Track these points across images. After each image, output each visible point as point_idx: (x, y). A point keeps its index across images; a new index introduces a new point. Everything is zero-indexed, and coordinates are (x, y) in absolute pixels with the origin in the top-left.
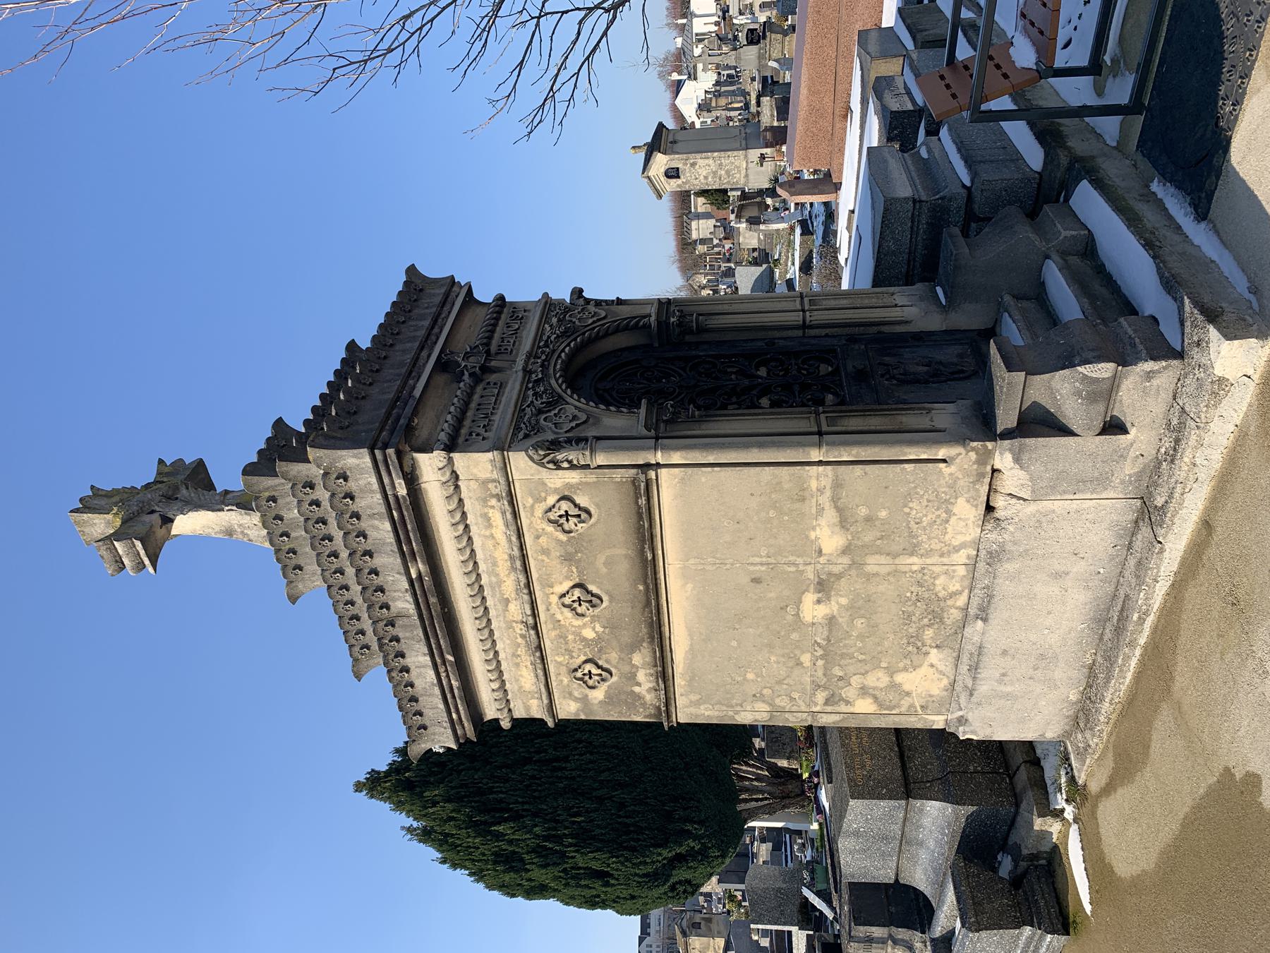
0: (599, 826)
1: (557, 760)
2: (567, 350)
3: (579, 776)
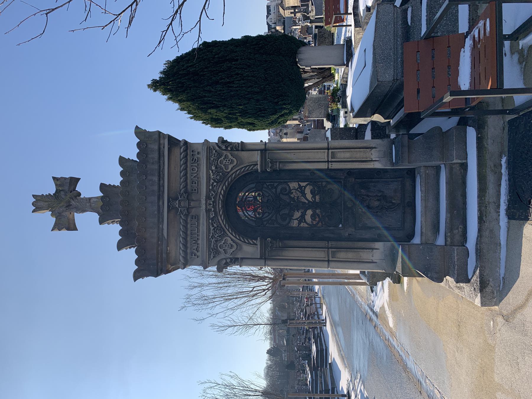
1: (229, 83)
2: (222, 192)
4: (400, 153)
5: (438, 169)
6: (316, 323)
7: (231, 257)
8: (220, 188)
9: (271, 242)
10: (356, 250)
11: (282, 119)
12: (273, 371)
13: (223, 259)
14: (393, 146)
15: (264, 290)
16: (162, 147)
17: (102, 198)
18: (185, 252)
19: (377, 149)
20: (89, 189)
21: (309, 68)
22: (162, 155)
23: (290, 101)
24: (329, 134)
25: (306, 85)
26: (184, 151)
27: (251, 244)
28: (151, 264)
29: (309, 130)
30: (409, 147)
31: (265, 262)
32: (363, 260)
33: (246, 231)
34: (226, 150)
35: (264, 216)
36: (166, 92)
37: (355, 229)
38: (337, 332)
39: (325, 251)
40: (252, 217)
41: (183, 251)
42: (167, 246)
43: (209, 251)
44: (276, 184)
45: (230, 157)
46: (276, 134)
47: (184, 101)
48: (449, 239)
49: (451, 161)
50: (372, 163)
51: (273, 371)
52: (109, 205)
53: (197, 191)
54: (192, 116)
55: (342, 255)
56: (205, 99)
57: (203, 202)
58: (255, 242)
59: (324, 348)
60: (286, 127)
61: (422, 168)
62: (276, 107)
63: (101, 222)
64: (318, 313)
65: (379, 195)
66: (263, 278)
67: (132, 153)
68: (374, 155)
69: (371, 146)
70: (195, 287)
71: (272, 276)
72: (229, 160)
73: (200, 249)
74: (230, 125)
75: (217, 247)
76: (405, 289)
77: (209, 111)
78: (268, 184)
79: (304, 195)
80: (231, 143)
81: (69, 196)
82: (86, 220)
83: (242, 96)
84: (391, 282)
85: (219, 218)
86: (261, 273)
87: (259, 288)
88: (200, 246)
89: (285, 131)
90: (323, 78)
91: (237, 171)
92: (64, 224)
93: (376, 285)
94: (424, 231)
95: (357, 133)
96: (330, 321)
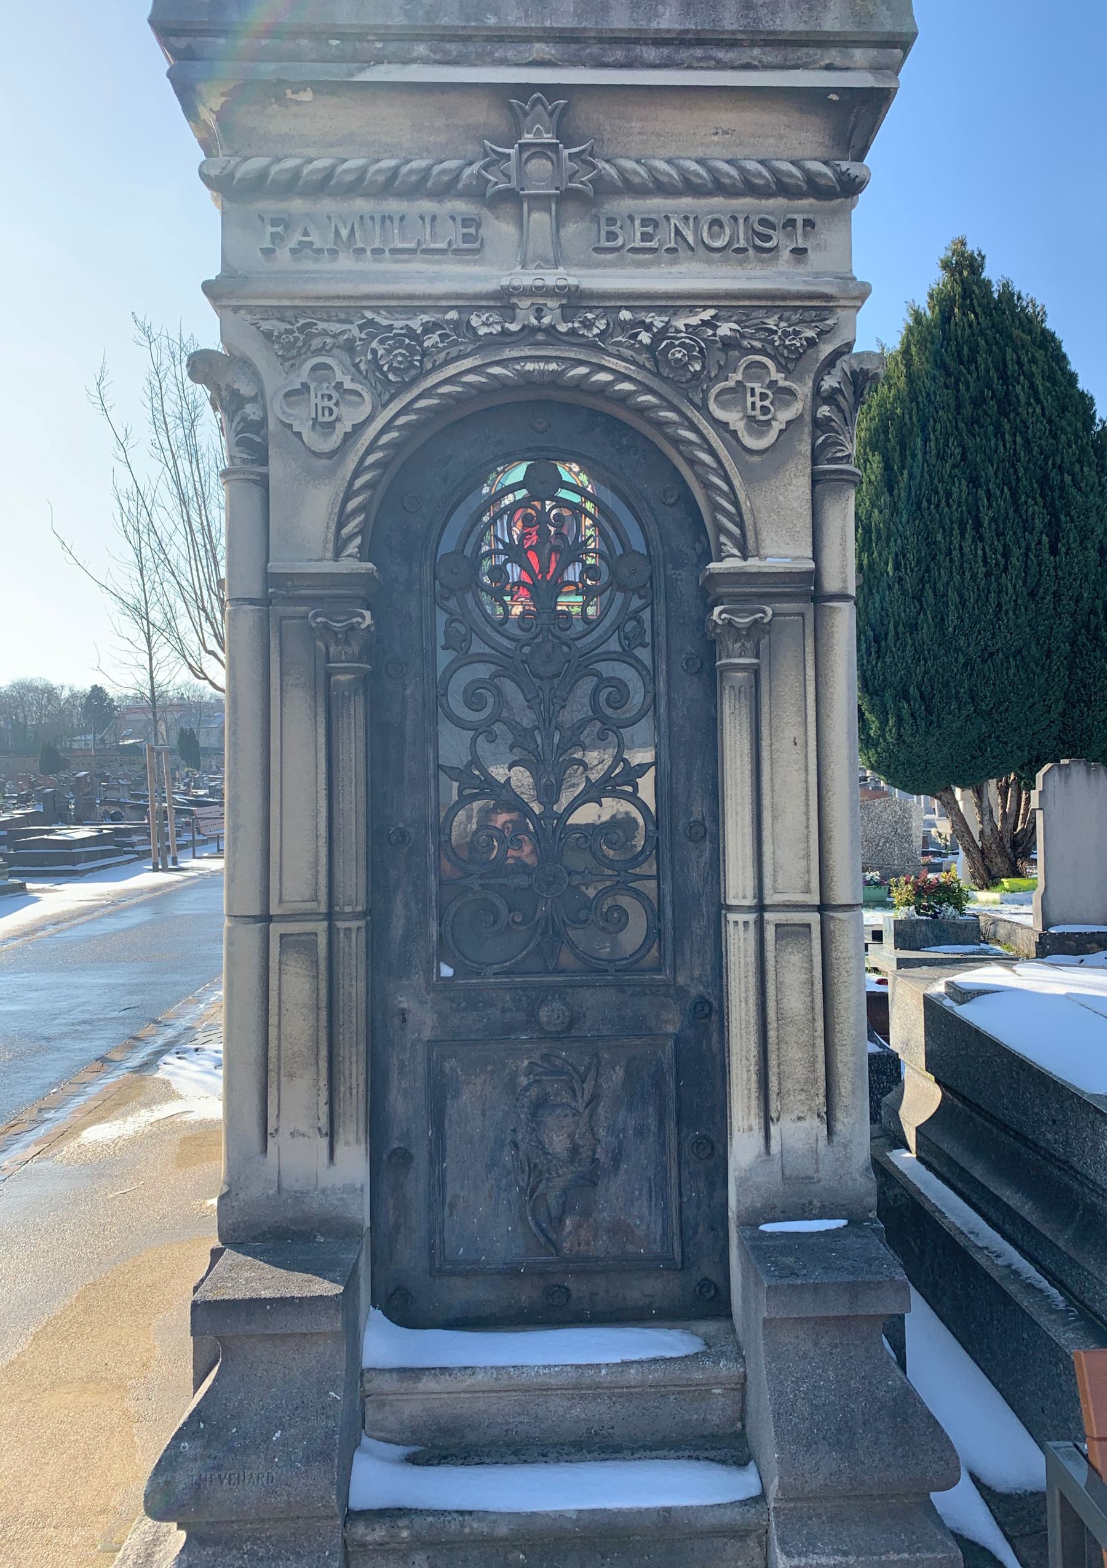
0: (883, 599)
1: (978, 525)
2: (603, 377)
3: (952, 561)
5: (728, 1447)
6: (163, 837)
7: (272, 426)
9: (352, 627)
10: (324, 1052)
12: (40, 707)
13: (256, 377)
14: (843, 1223)
16: (833, 56)
18: (291, 186)
19: (822, 1144)
21: (1035, 803)
22: (793, 54)
23: (909, 740)
25: (958, 792)
26: (810, 178)
27: (340, 526)
30: (842, 1322)
31: (251, 601)
32: (272, 1091)
33: (411, 504)
34: (819, 397)
36: (940, 302)
38: (123, 910)
39: (315, 899)
43: (301, 311)
44: (644, 654)
45: (784, 416)
47: (908, 366)
48: (379, 1533)
49: (782, 1541)
50: (756, 1123)
51: (40, 707)
53: (608, 250)
55: (297, 986)
56: (919, 442)
57: (551, 278)
58: (352, 548)
59: (80, 867)
61: (736, 1369)
62: (888, 694)
64: (204, 842)
68: (798, 1131)
69: (840, 1114)
72: (765, 410)
73: (308, 265)
75: (318, 352)
77: (876, 459)
78: (646, 615)
79: (594, 793)
83: (928, 570)
85: (468, 363)
88: (325, 265)
90: (982, 852)
91: (712, 452)
94: (427, 1384)
96: (169, 885)
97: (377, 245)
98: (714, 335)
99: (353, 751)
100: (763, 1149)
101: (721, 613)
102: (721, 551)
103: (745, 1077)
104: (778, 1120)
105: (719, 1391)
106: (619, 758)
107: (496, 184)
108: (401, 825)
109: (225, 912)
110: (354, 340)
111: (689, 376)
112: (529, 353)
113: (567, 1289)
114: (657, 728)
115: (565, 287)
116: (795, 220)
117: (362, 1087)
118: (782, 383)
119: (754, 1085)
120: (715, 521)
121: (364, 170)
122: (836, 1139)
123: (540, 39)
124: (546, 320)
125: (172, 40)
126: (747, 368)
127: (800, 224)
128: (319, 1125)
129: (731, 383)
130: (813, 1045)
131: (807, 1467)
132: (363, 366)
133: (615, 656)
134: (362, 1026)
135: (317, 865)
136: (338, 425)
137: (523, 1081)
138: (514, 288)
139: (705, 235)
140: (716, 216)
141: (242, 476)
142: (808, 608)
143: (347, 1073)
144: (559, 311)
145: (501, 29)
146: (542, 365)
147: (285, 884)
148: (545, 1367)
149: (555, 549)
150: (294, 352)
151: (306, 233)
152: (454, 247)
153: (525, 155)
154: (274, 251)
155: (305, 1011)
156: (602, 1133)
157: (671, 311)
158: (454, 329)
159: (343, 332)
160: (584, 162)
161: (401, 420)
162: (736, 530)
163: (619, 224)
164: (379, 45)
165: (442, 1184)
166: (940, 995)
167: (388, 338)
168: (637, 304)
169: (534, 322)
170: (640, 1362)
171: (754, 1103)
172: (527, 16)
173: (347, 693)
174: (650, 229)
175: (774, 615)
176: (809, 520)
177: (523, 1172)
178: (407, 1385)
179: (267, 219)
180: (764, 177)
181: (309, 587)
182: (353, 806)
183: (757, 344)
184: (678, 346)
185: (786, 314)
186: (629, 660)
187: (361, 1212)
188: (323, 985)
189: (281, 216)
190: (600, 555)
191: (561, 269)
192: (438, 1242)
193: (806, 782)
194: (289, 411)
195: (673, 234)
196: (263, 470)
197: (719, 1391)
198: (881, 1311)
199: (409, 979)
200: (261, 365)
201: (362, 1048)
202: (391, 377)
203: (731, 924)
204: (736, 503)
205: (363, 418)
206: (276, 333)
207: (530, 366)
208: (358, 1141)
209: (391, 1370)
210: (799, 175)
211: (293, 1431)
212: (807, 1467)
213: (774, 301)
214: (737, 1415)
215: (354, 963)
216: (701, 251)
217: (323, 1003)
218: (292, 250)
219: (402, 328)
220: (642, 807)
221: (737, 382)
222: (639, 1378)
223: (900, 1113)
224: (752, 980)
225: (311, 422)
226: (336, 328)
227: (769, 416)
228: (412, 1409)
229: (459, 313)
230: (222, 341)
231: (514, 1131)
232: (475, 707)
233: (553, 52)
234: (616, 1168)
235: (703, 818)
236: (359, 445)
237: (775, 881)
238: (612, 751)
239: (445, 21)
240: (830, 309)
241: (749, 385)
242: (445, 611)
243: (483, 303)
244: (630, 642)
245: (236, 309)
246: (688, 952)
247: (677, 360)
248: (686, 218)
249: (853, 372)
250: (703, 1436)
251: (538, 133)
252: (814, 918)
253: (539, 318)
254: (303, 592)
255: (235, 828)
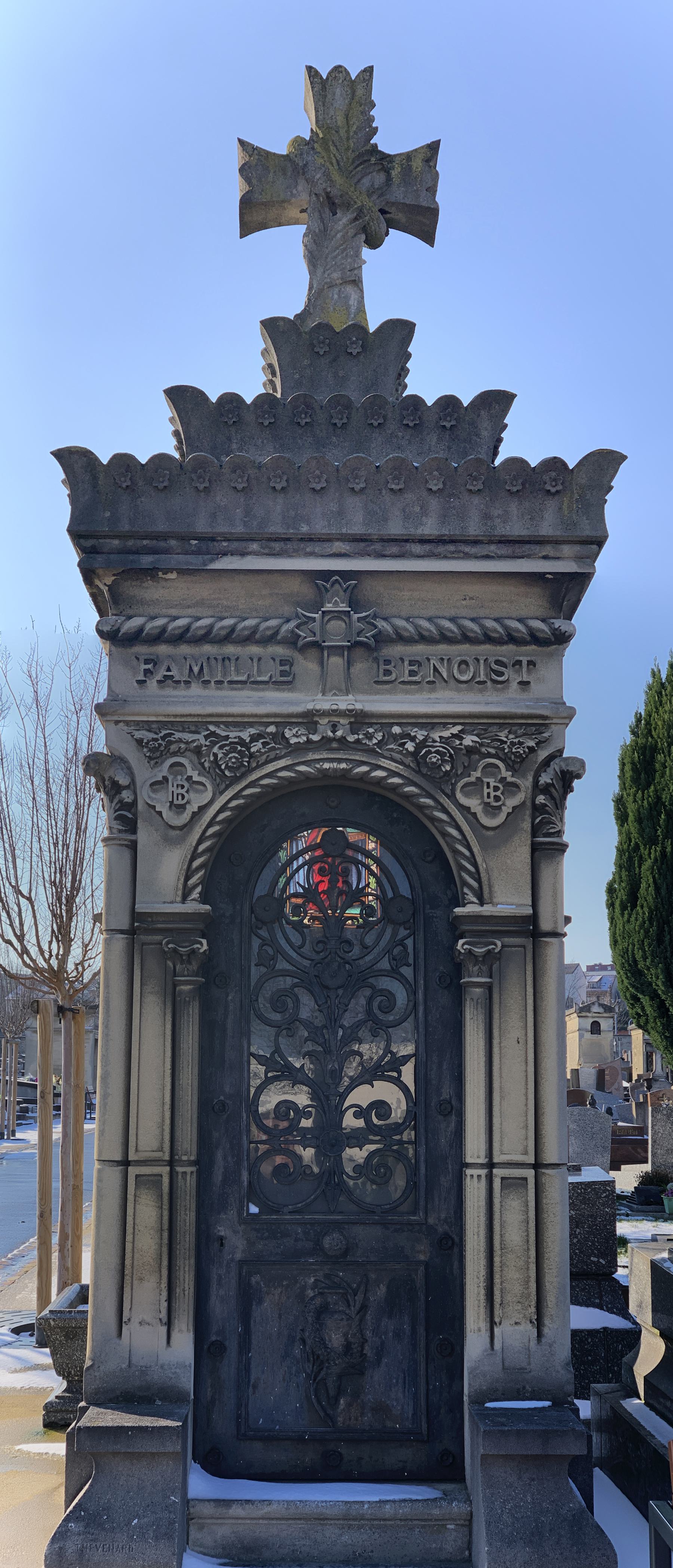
4: (522, 1426)
7: (140, 806)
8: (393, 766)
9: (193, 951)
10: (165, 1263)
11: (649, 1010)
14: (547, 1404)
15: (21, 938)
16: (548, 550)
17: (360, 328)
18: (159, 637)
19: (533, 1342)
20: (392, 279)
24: (592, 1174)
27: (187, 878)
28: (118, 520)
29: (609, 1111)
31: (122, 932)
32: (127, 1290)
33: (235, 857)
34: (537, 788)
35: (288, 929)
37: (242, 1263)
39: (161, 1149)
40: (287, 883)
41: (164, 629)
42: (181, 572)
43: (163, 724)
44: (407, 972)
45: (512, 802)
46: (595, 990)
50: (484, 1325)
52: (336, 361)
53: (383, 682)
54: (664, 676)
55: (147, 1213)
57: (344, 703)
58: (195, 894)
60: (622, 1030)
61: (464, 1508)
63: (271, 326)
65: (367, 1350)
66: (63, 933)
67: (525, 440)
68: (515, 1332)
69: (547, 1321)
70: (35, 684)
71: (70, 967)
72: (497, 799)
73: (169, 691)
74: (631, 818)
75: (175, 754)
76: (25, 1447)
78: (409, 942)
80: (560, 805)
81: (368, 203)
82: (279, 272)
84: (51, 1398)
85: (282, 763)
86: (82, 926)
87: (28, 921)
88: (181, 692)
89: (606, 1024)
92: (266, 189)
93: (41, 1344)
94: (236, 1511)
95: (595, 1279)
97: (219, 678)
98: (461, 744)
99: (191, 1042)
100: (488, 1345)
101: (463, 945)
102: (464, 898)
103: (476, 1291)
104: (500, 1324)
105: (452, 1527)
106: (388, 1050)
107: (305, 638)
108: (222, 1098)
109: (95, 1157)
110: (201, 746)
111: (442, 774)
112: (326, 756)
113: (340, 1454)
114: (417, 1028)
115: (353, 710)
116: (521, 661)
117: (192, 1290)
118: (509, 779)
119: (482, 1297)
120: (461, 877)
121: (211, 626)
122: (544, 1340)
123: (338, 540)
124: (339, 733)
125: (82, 541)
126: (484, 767)
127: (525, 663)
128: (161, 1316)
129: (472, 779)
130: (528, 1269)
131: (508, 1557)
132: (207, 765)
133: (386, 973)
134: (193, 1246)
135: (163, 1125)
136: (188, 806)
137: (310, 1293)
138: (317, 711)
139: (455, 672)
140: (463, 658)
141: (119, 842)
142: (528, 942)
143: (182, 1279)
144: (348, 726)
145: (311, 534)
146: (335, 764)
147: (140, 1137)
148: (322, 1502)
149: (341, 893)
150: (158, 754)
151: (169, 670)
152: (274, 680)
153: (326, 618)
154: (145, 681)
155: (152, 1232)
156: (368, 1334)
157: (430, 727)
158: (273, 739)
159: (193, 741)
160: (369, 623)
161: (234, 803)
162: (475, 884)
163: (393, 664)
164: (225, 544)
165: (248, 1370)
166: (664, 1260)
167: (225, 745)
168: (405, 721)
169: (330, 734)
170: (394, 1501)
171: (482, 1310)
172: (329, 525)
173: (187, 999)
174: (415, 668)
175: (503, 946)
176: (529, 877)
177: (309, 1361)
178: (221, 1511)
179: (142, 658)
180: (498, 632)
181: (164, 922)
182: (190, 1082)
183: (492, 751)
184: (435, 752)
185: (514, 728)
186: (395, 976)
187: (188, 1383)
188: (166, 1213)
189: (152, 657)
190: (377, 898)
191: (350, 697)
192: (244, 1413)
193: (526, 1071)
194: (153, 796)
195: (432, 671)
196: (133, 837)
197: (452, 1527)
198: (565, 1452)
199: (226, 1214)
200: (133, 763)
201: (193, 1261)
202: (227, 773)
203: (469, 1177)
204: (475, 865)
205: (206, 801)
206: (145, 741)
207: (326, 766)
208: (188, 1330)
209: (209, 1501)
210: (524, 631)
211: (146, 1519)
212: (508, 1557)
213: (504, 720)
214: (465, 1546)
215: (188, 1198)
216: (452, 683)
217: (166, 1226)
218: (159, 682)
219: (235, 738)
220: (404, 1089)
221: (477, 778)
222: (392, 1512)
223: (634, 1368)
224: (483, 1219)
225: (168, 804)
226: (189, 737)
227: (500, 803)
228: (223, 1531)
229: (277, 727)
230: (106, 744)
231: (302, 1330)
232: (280, 1010)
233: (348, 548)
234: (379, 1362)
235: (451, 1098)
236: (202, 821)
237: (501, 1145)
238: (382, 1045)
239: (272, 529)
240: (546, 725)
241: (486, 780)
242: (259, 937)
243: (294, 720)
244: (398, 961)
245: (117, 722)
246: (437, 1199)
247: (433, 763)
248: (442, 659)
249: (562, 772)
250: (440, 1561)
251: (336, 604)
252: (530, 1173)
253: (334, 732)
254: (159, 926)
255: (105, 1097)
